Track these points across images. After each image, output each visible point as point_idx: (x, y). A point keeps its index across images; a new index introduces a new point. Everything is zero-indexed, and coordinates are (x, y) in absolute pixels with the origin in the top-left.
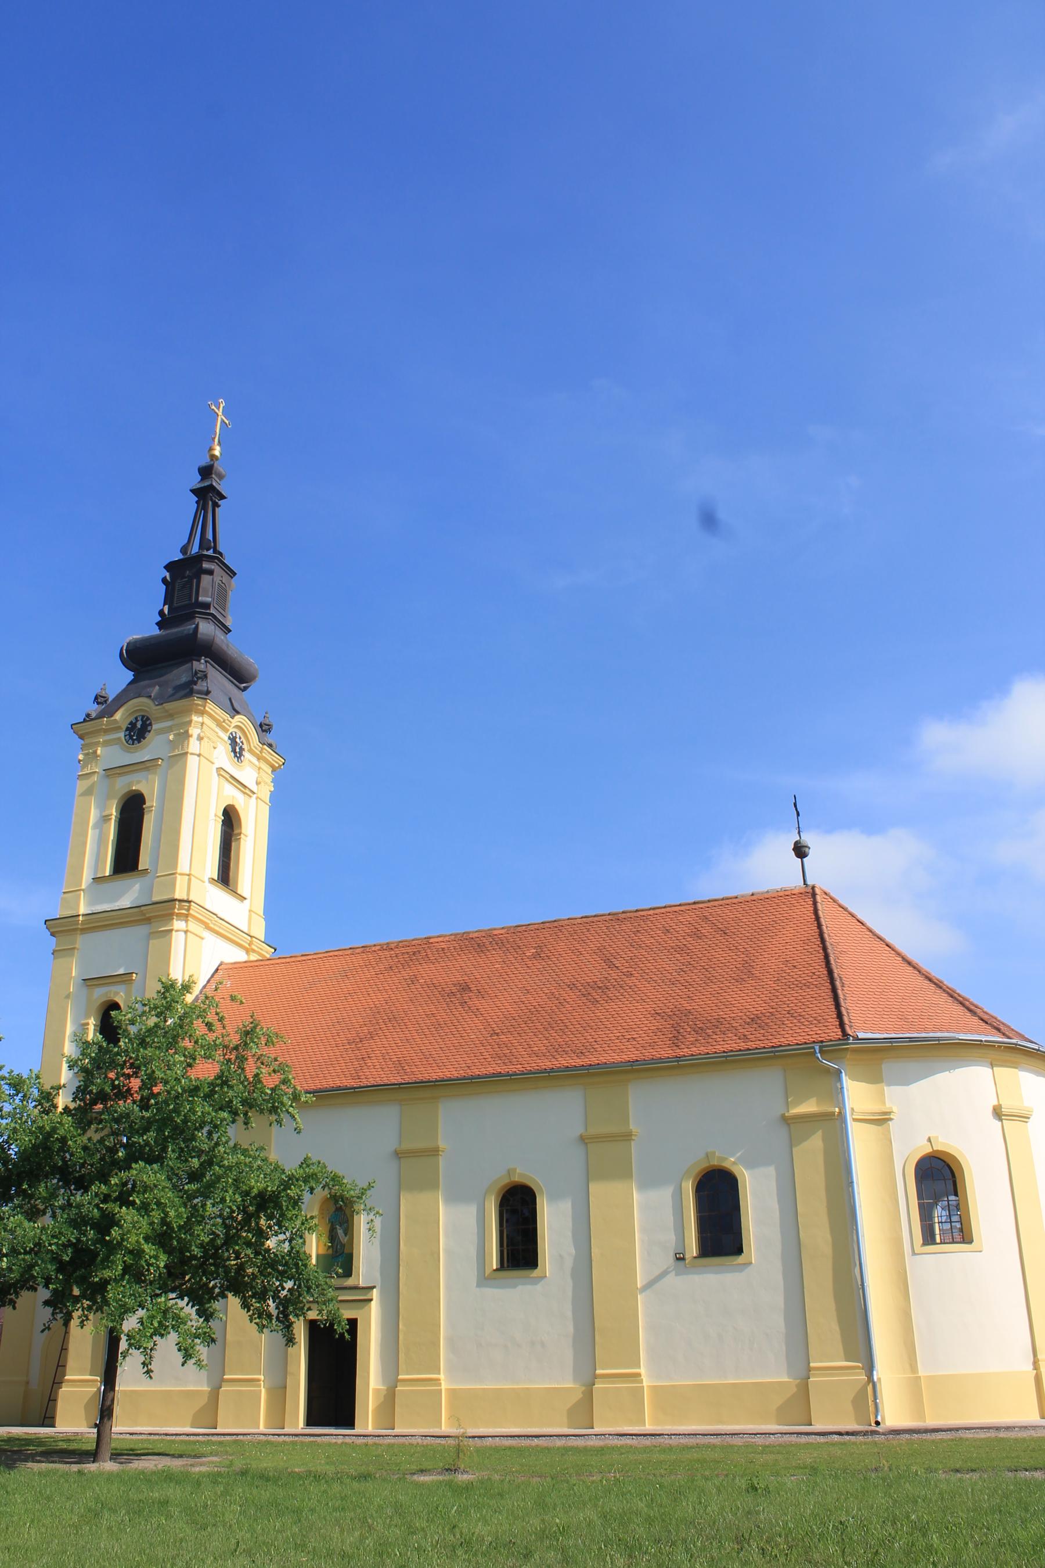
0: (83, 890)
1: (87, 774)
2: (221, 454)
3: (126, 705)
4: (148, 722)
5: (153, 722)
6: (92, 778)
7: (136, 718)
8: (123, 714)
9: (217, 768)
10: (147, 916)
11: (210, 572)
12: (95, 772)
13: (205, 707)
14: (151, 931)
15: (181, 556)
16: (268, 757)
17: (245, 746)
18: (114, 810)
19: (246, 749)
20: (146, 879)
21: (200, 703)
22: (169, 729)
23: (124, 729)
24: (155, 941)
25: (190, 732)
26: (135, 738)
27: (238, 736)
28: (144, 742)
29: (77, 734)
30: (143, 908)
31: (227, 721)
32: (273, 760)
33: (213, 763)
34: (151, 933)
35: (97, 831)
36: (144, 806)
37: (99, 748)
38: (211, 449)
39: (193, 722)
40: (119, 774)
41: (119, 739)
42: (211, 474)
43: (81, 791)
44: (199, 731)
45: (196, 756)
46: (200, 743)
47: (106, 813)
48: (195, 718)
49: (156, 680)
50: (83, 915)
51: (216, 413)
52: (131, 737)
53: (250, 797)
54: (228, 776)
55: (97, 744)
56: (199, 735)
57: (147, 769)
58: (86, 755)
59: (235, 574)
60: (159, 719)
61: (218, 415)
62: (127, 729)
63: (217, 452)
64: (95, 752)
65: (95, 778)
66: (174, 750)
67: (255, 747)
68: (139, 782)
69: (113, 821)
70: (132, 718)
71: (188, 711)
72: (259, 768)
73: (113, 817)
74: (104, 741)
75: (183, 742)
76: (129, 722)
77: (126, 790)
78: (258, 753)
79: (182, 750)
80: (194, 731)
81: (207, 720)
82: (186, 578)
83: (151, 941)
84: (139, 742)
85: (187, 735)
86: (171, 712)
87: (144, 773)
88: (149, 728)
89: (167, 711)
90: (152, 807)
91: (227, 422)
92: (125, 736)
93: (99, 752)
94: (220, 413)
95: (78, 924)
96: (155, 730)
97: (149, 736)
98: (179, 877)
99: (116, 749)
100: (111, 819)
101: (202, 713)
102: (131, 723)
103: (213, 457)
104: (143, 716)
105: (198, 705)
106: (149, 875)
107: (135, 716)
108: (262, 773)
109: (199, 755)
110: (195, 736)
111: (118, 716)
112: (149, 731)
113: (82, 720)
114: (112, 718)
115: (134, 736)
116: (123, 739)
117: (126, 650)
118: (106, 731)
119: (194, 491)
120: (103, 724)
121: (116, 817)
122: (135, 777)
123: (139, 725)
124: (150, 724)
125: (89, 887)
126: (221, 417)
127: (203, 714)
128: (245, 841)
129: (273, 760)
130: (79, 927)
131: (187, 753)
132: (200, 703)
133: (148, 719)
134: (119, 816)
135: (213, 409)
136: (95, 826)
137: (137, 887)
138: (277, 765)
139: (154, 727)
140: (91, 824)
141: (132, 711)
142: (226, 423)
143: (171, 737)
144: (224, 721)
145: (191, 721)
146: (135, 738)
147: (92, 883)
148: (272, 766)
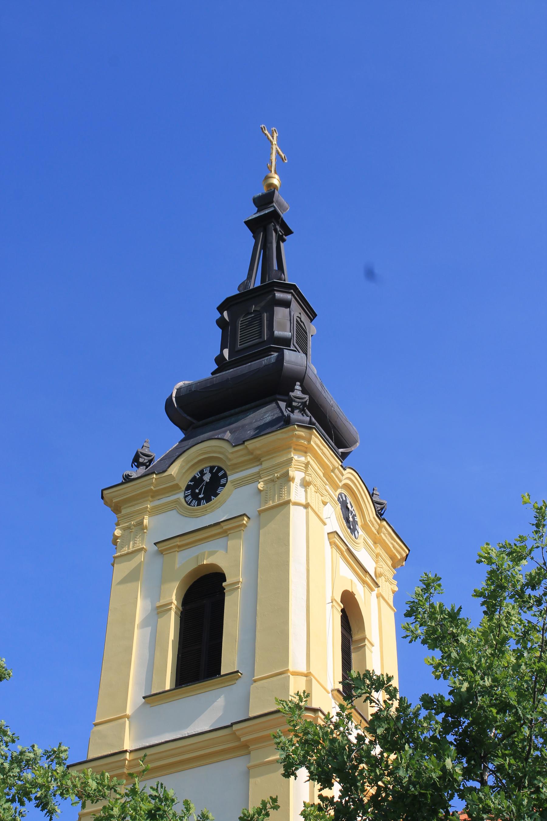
0: (128, 717)
1: (128, 554)
2: (280, 186)
3: (183, 455)
4: (220, 474)
5: (228, 473)
6: (139, 556)
7: (202, 472)
8: (181, 467)
9: (328, 534)
10: (243, 739)
11: (286, 304)
12: (142, 549)
13: (309, 441)
14: (252, 763)
15: (238, 292)
16: (388, 541)
17: (358, 519)
18: (174, 597)
19: (359, 523)
20: (238, 687)
21: (302, 434)
22: (257, 477)
23: (184, 489)
24: (258, 780)
25: (291, 473)
26: (200, 496)
27: (348, 501)
28: (214, 500)
29: (110, 506)
30: (235, 727)
31: (336, 471)
32: (394, 547)
33: (325, 524)
34: (249, 768)
35: (149, 630)
36: (224, 584)
37: (146, 517)
38: (267, 178)
39: (294, 460)
40: (179, 547)
41: (177, 501)
42: (272, 202)
43: (119, 580)
44: (302, 475)
45: (302, 508)
46: (306, 492)
47: (163, 602)
48: (298, 458)
49: (227, 427)
50: (131, 752)
51: (271, 141)
52: (195, 496)
53: (372, 590)
54: (344, 548)
55: (144, 511)
56: (303, 480)
57: (225, 533)
58: (124, 529)
59: (315, 315)
60: (236, 467)
61: (272, 144)
62: (188, 488)
63: (276, 181)
64: (142, 522)
65: (141, 557)
66: (266, 502)
67: (370, 521)
68: (212, 553)
69: (173, 613)
70: (195, 473)
71: (286, 448)
72: (378, 555)
73: (173, 606)
74: (153, 508)
75: (281, 489)
76: (190, 478)
77: (192, 566)
78: (375, 532)
79: (279, 500)
80: (297, 475)
81: (310, 458)
82: (251, 313)
83: (252, 781)
84: (208, 500)
85: (287, 479)
86: (258, 452)
87: (221, 541)
88: (223, 481)
89: (250, 453)
90: (238, 583)
91: (283, 156)
92: (185, 497)
93: (146, 522)
94: (275, 142)
95: (123, 766)
96: (232, 482)
97: (223, 492)
98: (291, 677)
99: (173, 515)
100: (170, 609)
101: (305, 451)
102: (194, 479)
103: (271, 185)
104: (212, 468)
105: (299, 437)
106: (239, 682)
107: (200, 469)
108: (382, 563)
109: (306, 506)
110: (298, 481)
111: (174, 470)
112: (224, 485)
113: (121, 480)
114: (166, 474)
115: (200, 493)
116: (183, 500)
117: (176, 397)
118: (155, 494)
119: (250, 224)
120: (152, 484)
121: (177, 607)
122: (205, 547)
123: (207, 478)
124: (225, 476)
125: (139, 711)
126: (275, 147)
127: (306, 453)
128: (371, 652)
129: (394, 547)
130: (126, 771)
131: (288, 502)
132: (302, 434)
133: (220, 469)
134: (181, 609)
135: (265, 134)
136: (144, 624)
137: (220, 702)
138: (399, 557)
139: (230, 478)
140: (138, 621)
141: (196, 460)
142: (280, 156)
143: (261, 486)
144: (333, 471)
145: (291, 459)
146: (200, 496)
147: (144, 704)
148: (392, 557)
